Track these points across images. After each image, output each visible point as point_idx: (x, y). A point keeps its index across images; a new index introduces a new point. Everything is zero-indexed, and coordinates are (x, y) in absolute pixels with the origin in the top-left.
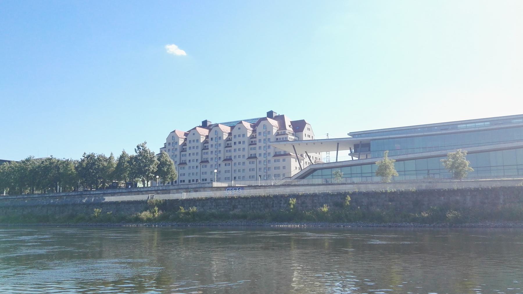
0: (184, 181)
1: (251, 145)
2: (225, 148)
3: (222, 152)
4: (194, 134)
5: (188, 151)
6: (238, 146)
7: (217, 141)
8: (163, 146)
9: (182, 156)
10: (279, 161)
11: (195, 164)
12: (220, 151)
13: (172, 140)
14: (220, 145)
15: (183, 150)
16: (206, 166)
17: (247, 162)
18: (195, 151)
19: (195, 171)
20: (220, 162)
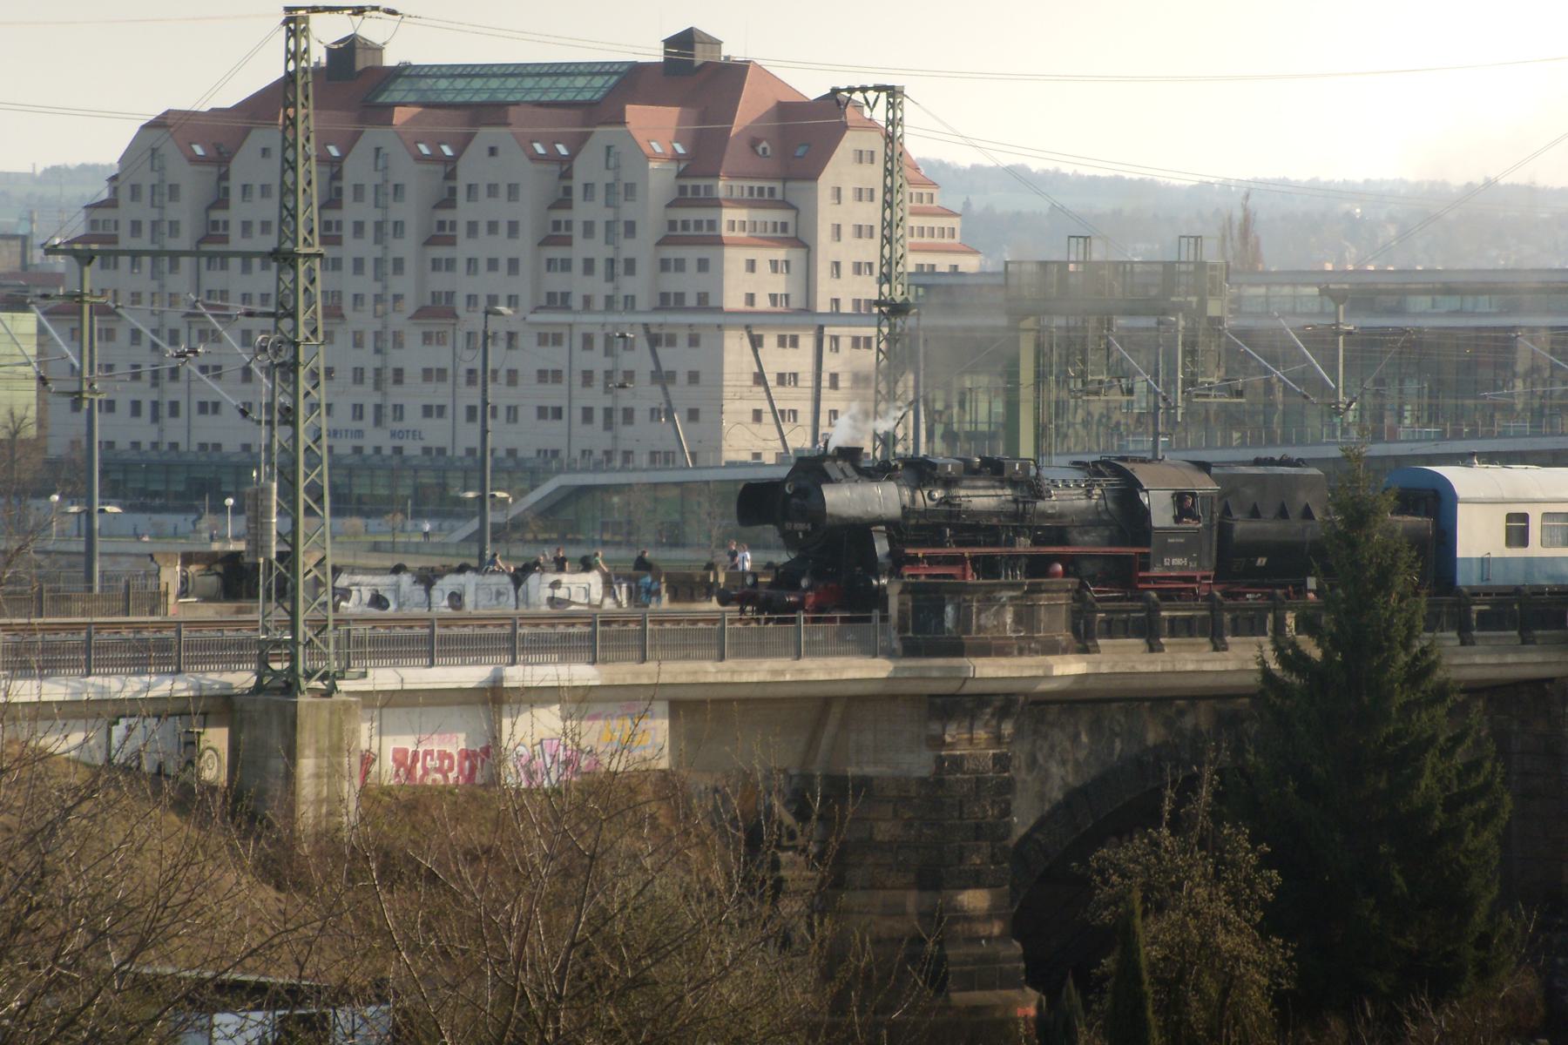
0: (542, 412)
1: (668, 244)
4: (493, 151)
6: (482, 247)
7: (162, 208)
8: (105, 195)
13: (607, 168)
14: (177, 230)
18: (502, 247)
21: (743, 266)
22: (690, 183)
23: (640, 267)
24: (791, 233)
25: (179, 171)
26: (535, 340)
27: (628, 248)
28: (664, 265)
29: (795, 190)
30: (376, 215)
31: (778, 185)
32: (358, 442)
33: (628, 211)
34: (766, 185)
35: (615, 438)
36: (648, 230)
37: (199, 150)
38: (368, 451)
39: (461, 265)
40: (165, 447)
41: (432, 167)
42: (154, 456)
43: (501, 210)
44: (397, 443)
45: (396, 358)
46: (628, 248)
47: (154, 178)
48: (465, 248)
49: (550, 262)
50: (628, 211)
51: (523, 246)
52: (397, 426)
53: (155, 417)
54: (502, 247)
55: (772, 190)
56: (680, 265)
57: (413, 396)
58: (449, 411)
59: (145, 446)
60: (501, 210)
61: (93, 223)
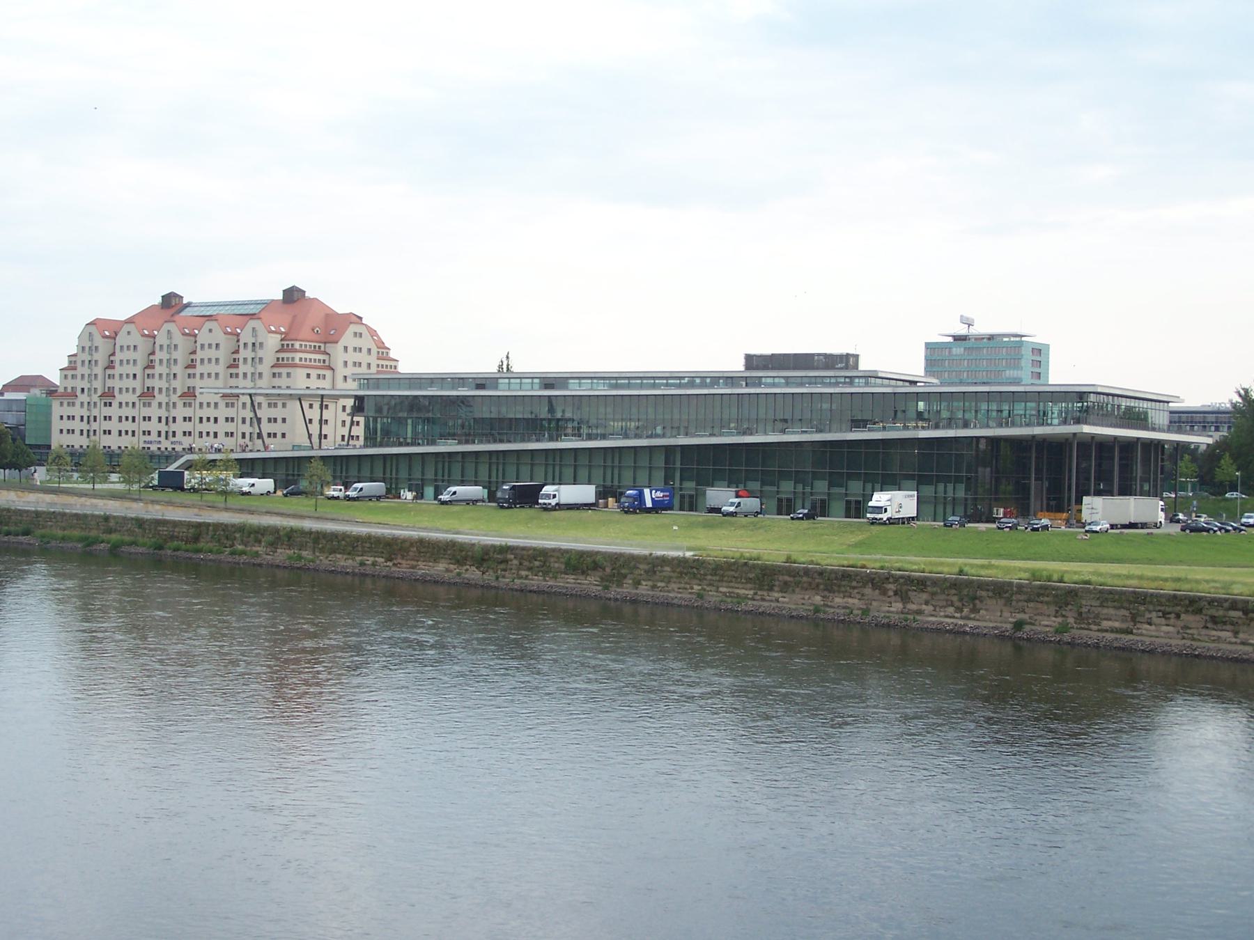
0: (149, 433)
2: (186, 368)
3: (100, 377)
5: (118, 370)
7: (170, 353)
9: (109, 378)
10: (275, 405)
11: (132, 398)
12: (260, 374)
15: (110, 365)
16: (150, 405)
18: (213, 368)
19: (129, 412)
21: (305, 376)
22: (285, 343)
23: (179, 376)
24: (327, 364)
25: (98, 341)
26: (224, 405)
27: (260, 368)
28: (274, 375)
29: (329, 348)
30: (167, 357)
31: (322, 345)
32: (159, 446)
33: (260, 353)
34: (317, 345)
35: (254, 444)
36: (269, 358)
37: (107, 333)
38: (163, 449)
39: (198, 376)
40: (65, 447)
41: (189, 338)
42: (81, 450)
43: (212, 353)
44: (173, 446)
45: (173, 413)
46: (260, 368)
47: (168, 342)
48: (199, 369)
49: (189, 374)
50: (260, 353)
51: (220, 369)
52: (174, 439)
54: (213, 368)
55: (320, 347)
57: (180, 427)
58: (235, 434)
59: (85, 447)
60: (212, 353)
61: (70, 362)
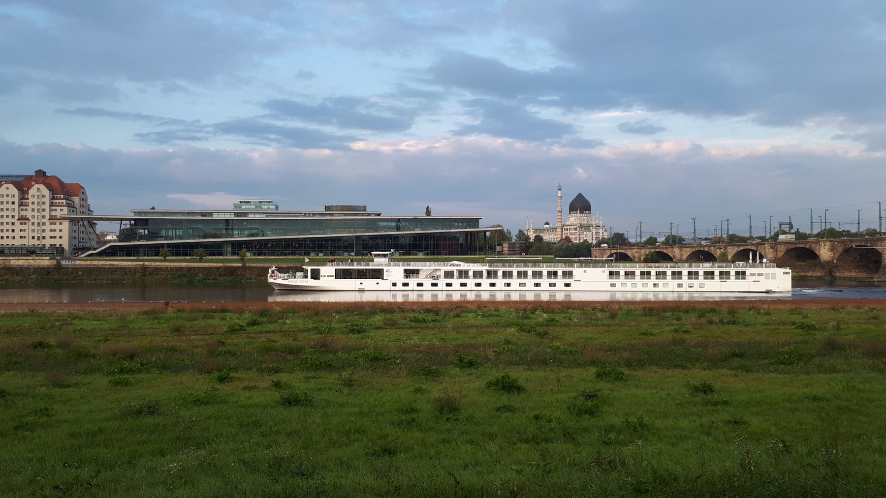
10: (55, 224)
17: (17, 223)
20: (44, 220)
28: (51, 210)
53: (38, 239)
56: (56, 210)
